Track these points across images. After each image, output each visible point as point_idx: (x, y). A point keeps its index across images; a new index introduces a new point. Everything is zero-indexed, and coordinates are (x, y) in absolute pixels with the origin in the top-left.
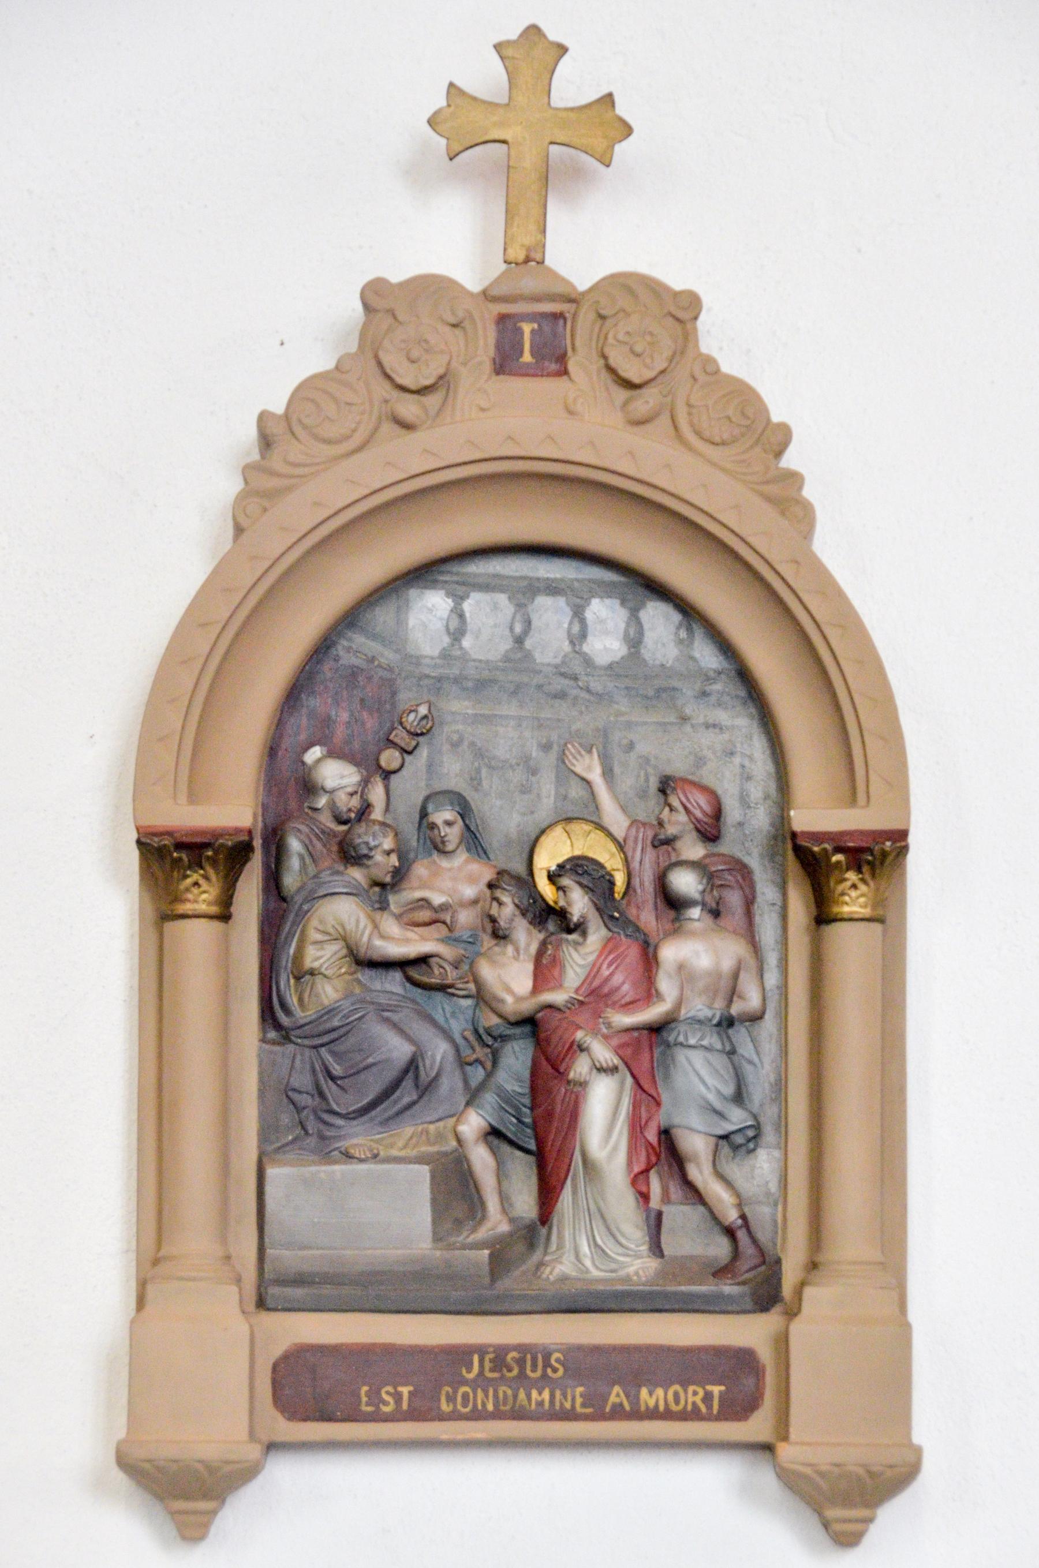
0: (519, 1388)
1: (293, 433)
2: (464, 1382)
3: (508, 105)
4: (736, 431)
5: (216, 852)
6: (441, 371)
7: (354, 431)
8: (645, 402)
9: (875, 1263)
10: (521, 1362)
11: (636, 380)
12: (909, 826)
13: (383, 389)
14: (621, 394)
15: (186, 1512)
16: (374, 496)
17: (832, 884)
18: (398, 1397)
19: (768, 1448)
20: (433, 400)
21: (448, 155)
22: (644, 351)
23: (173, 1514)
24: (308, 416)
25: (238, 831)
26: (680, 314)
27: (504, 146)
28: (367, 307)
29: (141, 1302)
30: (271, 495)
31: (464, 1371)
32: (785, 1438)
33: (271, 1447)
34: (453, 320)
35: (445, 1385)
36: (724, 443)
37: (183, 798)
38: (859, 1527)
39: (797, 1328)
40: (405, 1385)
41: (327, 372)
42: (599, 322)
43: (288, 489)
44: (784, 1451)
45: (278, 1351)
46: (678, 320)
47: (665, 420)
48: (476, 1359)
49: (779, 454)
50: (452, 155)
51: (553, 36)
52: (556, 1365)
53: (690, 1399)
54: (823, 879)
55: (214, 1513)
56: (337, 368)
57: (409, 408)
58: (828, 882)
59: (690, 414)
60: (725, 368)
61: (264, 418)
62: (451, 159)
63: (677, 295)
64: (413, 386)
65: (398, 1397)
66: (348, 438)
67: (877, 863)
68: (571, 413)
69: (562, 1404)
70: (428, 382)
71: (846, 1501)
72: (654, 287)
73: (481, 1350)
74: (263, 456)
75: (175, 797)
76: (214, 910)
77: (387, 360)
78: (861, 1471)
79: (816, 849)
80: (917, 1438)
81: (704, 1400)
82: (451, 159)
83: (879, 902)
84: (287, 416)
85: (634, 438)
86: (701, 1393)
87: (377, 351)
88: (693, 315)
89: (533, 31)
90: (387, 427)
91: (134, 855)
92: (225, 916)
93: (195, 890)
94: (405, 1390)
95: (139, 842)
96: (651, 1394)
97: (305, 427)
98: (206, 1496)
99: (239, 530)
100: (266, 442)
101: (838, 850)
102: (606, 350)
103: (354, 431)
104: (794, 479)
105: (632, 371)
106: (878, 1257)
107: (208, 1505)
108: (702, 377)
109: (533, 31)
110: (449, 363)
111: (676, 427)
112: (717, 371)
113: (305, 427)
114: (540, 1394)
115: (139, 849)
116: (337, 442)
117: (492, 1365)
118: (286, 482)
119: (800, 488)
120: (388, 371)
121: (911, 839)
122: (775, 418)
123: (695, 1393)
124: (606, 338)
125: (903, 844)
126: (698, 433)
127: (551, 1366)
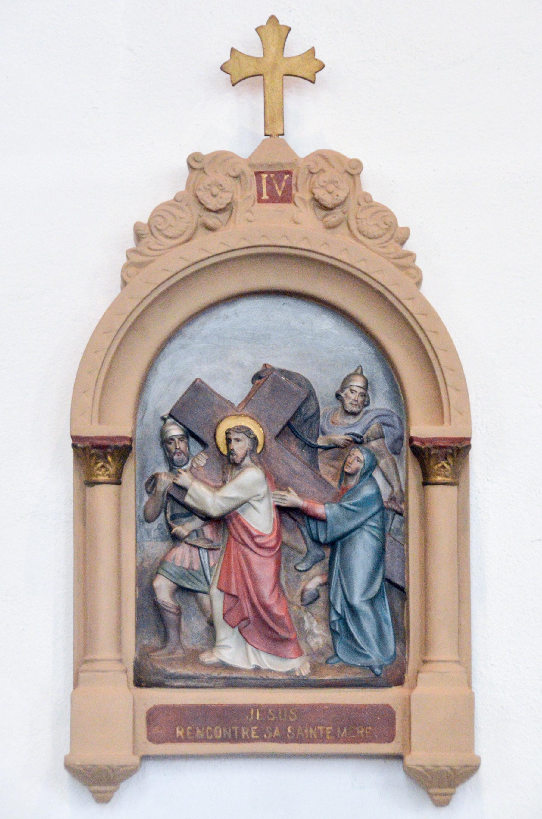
1: (152, 234)
6: (229, 201)
7: (184, 232)
8: (332, 219)
10: (277, 714)
12: (471, 434)
13: (196, 209)
15: (98, 792)
17: (432, 463)
19: (400, 757)
20: (223, 217)
22: (333, 191)
26: (353, 172)
28: (191, 168)
29: (76, 684)
30: (141, 265)
33: (145, 758)
34: (233, 174)
36: (375, 238)
37: (95, 424)
41: (345, 157)
42: (310, 175)
43: (152, 261)
47: (344, 226)
52: (292, 713)
54: (426, 461)
56: (175, 199)
57: (211, 220)
59: (357, 223)
62: (233, 85)
63: (350, 161)
64: (214, 209)
67: (455, 454)
68: (296, 223)
70: (222, 206)
71: (441, 785)
72: (339, 157)
74: (137, 246)
76: (113, 479)
77: (200, 194)
78: (447, 769)
82: (233, 85)
84: (149, 224)
90: (201, 230)
91: (70, 452)
92: (118, 482)
93: (103, 470)
95: (74, 446)
96: (314, 729)
97: (159, 230)
99: (125, 283)
100: (139, 237)
103: (184, 232)
107: (108, 788)
108: (363, 204)
110: (232, 197)
111: (349, 227)
113: (159, 230)
116: (180, 235)
119: (414, 261)
120: (202, 201)
121: (472, 442)
122: (401, 224)
124: (314, 184)
125: (467, 444)
126: (361, 232)
127: (291, 715)
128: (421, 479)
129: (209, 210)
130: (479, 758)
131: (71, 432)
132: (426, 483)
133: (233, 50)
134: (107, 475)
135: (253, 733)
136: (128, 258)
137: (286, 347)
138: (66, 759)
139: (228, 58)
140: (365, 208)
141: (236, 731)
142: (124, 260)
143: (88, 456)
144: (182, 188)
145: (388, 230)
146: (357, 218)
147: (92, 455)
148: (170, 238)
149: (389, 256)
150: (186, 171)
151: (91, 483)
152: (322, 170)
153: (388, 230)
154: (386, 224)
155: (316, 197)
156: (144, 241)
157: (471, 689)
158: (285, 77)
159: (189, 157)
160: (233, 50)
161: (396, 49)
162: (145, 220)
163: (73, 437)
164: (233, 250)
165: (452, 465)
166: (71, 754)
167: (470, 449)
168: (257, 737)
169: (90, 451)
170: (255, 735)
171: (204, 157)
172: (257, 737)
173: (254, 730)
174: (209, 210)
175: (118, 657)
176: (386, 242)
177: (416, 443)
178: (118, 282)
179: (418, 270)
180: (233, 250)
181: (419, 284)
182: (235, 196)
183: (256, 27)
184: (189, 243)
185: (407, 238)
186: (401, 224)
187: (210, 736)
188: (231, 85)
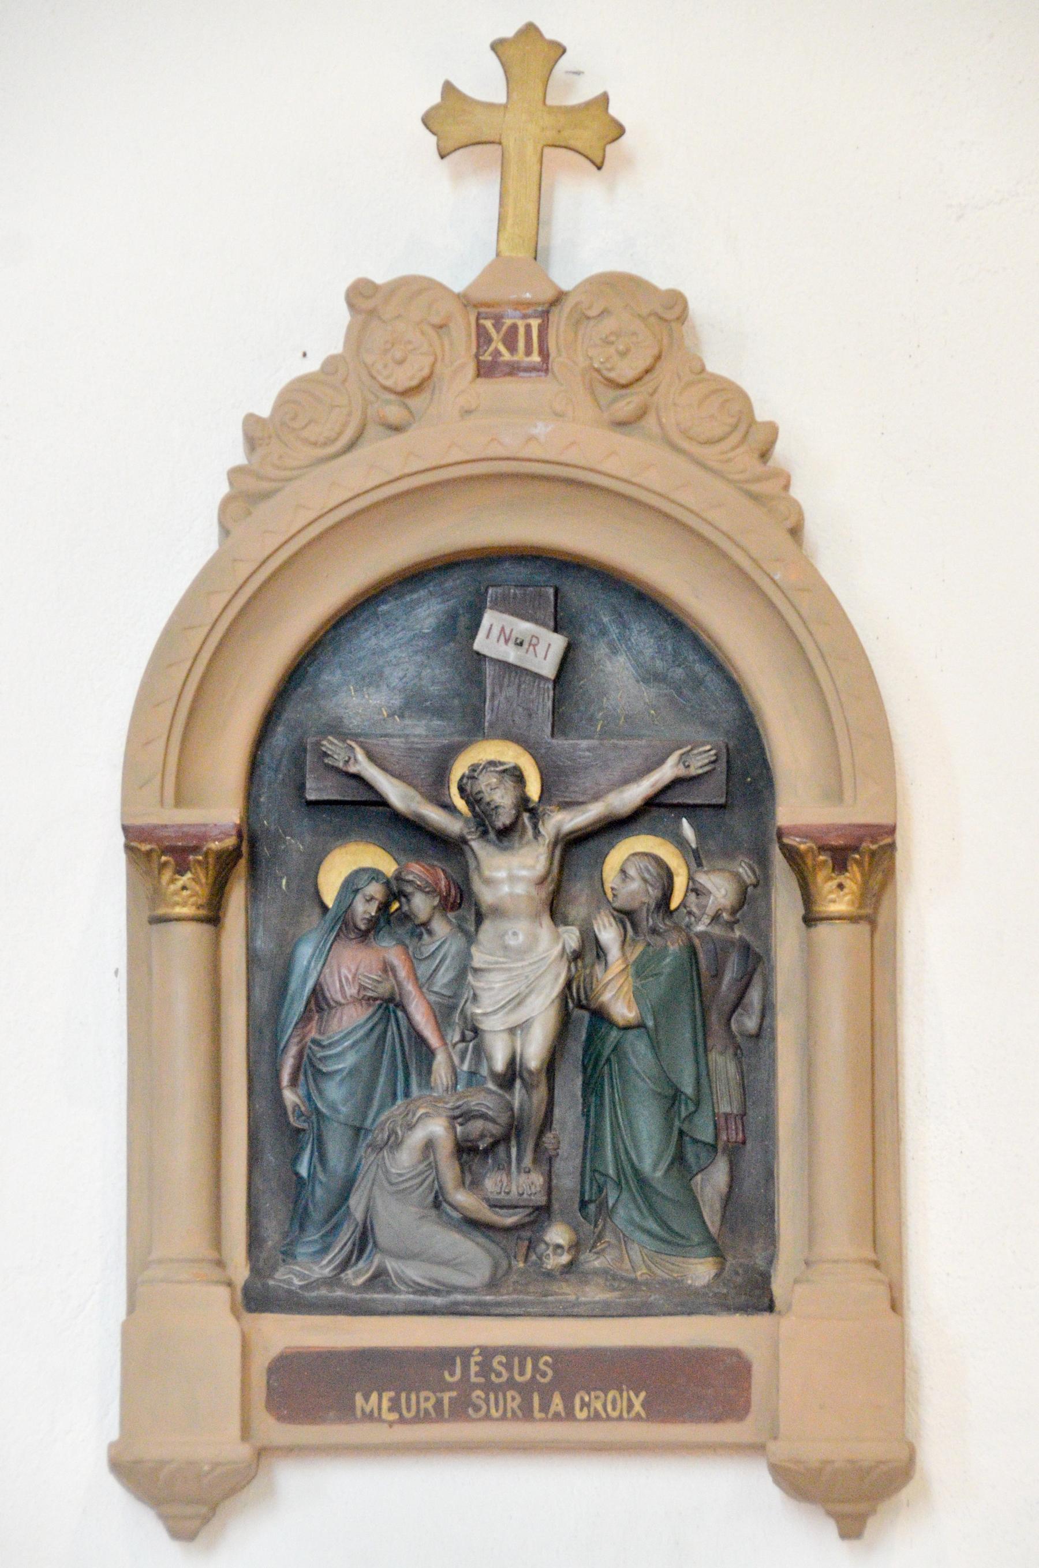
0: (371, 1392)
3: (505, 107)
4: (718, 431)
5: (206, 855)
6: (426, 372)
11: (623, 381)
16: (356, 501)
19: (756, 1449)
23: (164, 1517)
24: (294, 418)
26: (670, 315)
28: (351, 306)
33: (262, 1453)
34: (437, 320)
46: (661, 318)
48: (458, 1361)
49: (765, 455)
51: (549, 34)
53: (423, 1405)
58: (815, 878)
60: (710, 368)
61: (251, 421)
66: (340, 434)
70: (414, 383)
73: (466, 1353)
75: (162, 803)
76: (202, 912)
79: (802, 847)
81: (434, 1407)
82: (442, 157)
85: (618, 439)
86: (433, 1400)
87: (593, 366)
89: (530, 30)
91: (120, 858)
95: (129, 848)
99: (225, 531)
100: (252, 443)
101: (822, 849)
105: (626, 370)
106: (870, 1255)
109: (530, 30)
112: (703, 370)
114: (367, 1398)
115: (126, 853)
116: (325, 444)
117: (477, 1368)
118: (266, 486)
119: (786, 487)
123: (427, 1399)
127: (494, 1371)
128: (802, 911)
129: (625, 386)
132: (810, 920)
134: (193, 905)
136: (231, 483)
137: (585, 607)
138: (112, 1446)
140: (690, 384)
142: (225, 489)
143: (155, 866)
144: (337, 347)
145: (735, 427)
147: (165, 864)
148: (315, 444)
150: (342, 316)
152: (604, 313)
153: (735, 427)
154: (732, 416)
156: (260, 451)
158: (547, 150)
161: (954, 839)
162: (265, 411)
163: (125, 829)
164: (398, 479)
169: (160, 857)
170: (477, 1375)
171: (376, 288)
174: (625, 386)
176: (733, 449)
178: (215, 530)
180: (398, 479)
181: (796, 532)
182: (438, 365)
185: (772, 442)
186: (762, 414)
187: (581, 1410)
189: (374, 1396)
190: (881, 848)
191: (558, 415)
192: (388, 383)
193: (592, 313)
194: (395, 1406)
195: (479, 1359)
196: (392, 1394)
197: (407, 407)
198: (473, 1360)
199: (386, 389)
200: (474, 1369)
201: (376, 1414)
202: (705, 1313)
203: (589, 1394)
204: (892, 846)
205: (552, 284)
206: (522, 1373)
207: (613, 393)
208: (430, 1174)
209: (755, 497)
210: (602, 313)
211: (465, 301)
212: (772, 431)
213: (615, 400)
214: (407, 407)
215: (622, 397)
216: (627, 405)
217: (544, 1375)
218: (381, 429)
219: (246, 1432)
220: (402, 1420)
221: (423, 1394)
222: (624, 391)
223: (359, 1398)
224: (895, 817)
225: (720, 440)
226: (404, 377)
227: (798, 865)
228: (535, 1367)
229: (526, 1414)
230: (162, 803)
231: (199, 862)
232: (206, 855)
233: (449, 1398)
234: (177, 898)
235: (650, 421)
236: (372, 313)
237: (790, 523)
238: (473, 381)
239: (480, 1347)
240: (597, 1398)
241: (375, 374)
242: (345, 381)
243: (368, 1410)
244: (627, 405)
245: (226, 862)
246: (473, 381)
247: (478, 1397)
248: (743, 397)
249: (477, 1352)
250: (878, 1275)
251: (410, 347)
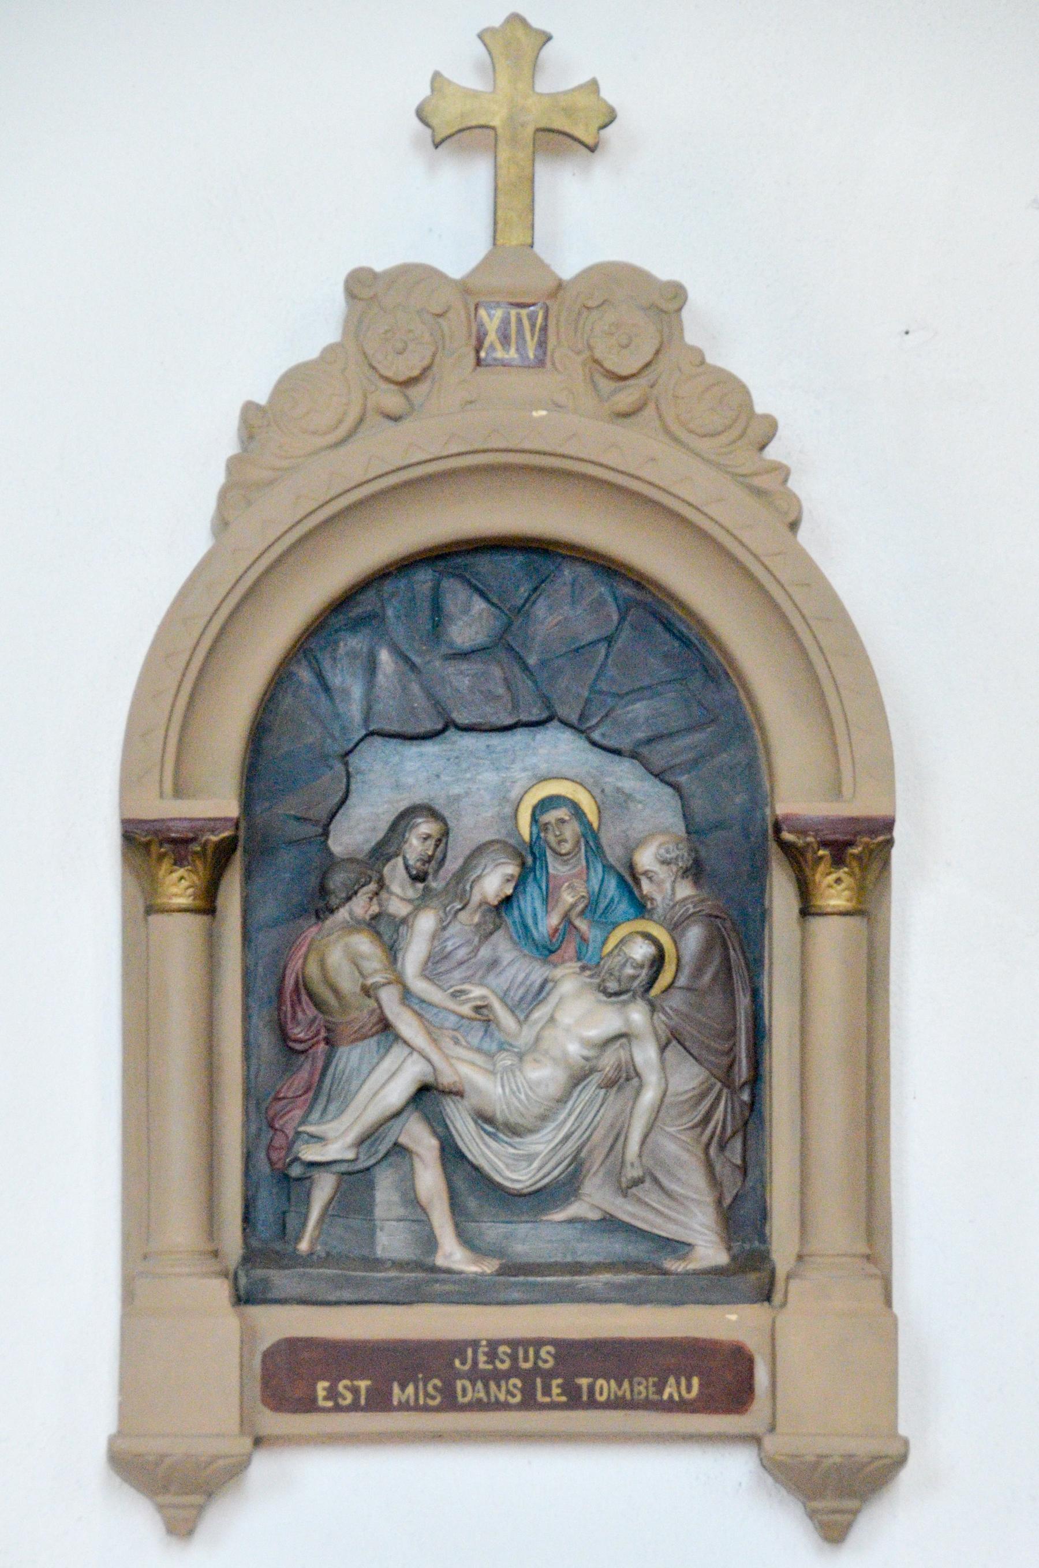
2: (460, 1375)
6: (426, 363)
9: (854, 1256)
11: (624, 372)
14: (606, 385)
18: (355, 1391)
21: (433, 141)
25: (214, 824)
26: (664, 305)
27: (492, 133)
31: (457, 1363)
32: (772, 1429)
33: (258, 1442)
35: (436, 1378)
36: (713, 435)
38: (847, 1517)
39: (784, 1320)
40: (362, 1378)
44: (770, 1443)
45: (266, 1343)
50: (438, 139)
54: (808, 872)
55: (855, 1512)
60: (709, 360)
61: (250, 410)
62: (437, 146)
65: (355, 1391)
69: (496, 1397)
70: (416, 373)
76: (199, 903)
80: (903, 1430)
82: (437, 146)
83: (861, 891)
85: (625, 434)
88: (676, 306)
89: (516, 19)
94: (363, 1384)
96: (499, 1387)
98: (852, 1494)
101: (824, 844)
102: (592, 342)
104: (782, 472)
106: (862, 1248)
107: (850, 1504)
109: (516, 19)
112: (703, 362)
114: (620, 1385)
116: (325, 433)
119: (785, 480)
121: (898, 832)
122: (759, 409)
125: (888, 837)
126: (683, 424)
127: (541, 1359)
128: (795, 906)
130: (906, 1443)
131: (121, 815)
132: (807, 911)
133: (437, 76)
135: (556, 1391)
139: (427, 92)
141: (363, 1392)
142: (219, 478)
146: (676, 397)
147: (161, 857)
149: (729, 469)
150: (337, 301)
151: (150, 910)
155: (598, 355)
157: (892, 1310)
159: (347, 282)
160: (437, 76)
165: (858, 877)
166: (121, 1433)
167: (892, 846)
168: (564, 1399)
172: (564, 1399)
173: (558, 1386)
175: (864, 1250)
177: (787, 836)
179: (794, 500)
181: (794, 526)
183: (478, 30)
184: (342, 450)
188: (431, 146)
189: (626, 1385)
190: (879, 844)
191: (558, 406)
192: (389, 374)
193: (590, 304)
194: (332, 1394)
195: (486, 1349)
196: (326, 1384)
197: (407, 397)
198: (481, 1350)
199: (387, 379)
200: (482, 1358)
201: (676, 1397)
202: (697, 1302)
203: (647, 1380)
204: (890, 843)
205: (552, 273)
206: (526, 1359)
207: (613, 385)
208: (706, 1234)
209: (759, 493)
210: (603, 304)
211: (465, 288)
212: (770, 428)
213: (614, 392)
214: (407, 397)
215: (621, 390)
216: (627, 397)
217: (546, 1361)
218: (380, 419)
219: (245, 1421)
220: (338, 1408)
221: (636, 1379)
222: (622, 384)
223: (396, 1388)
224: (895, 812)
225: (719, 433)
226: (405, 367)
227: (798, 862)
228: (537, 1356)
229: (529, 1403)
230: (162, 795)
231: (196, 853)
232: (204, 846)
233: (653, 1381)
234: (832, 891)
235: (650, 411)
236: (374, 297)
237: (791, 518)
238: (474, 370)
239: (553, 1342)
240: (639, 1384)
241: (375, 364)
242: (344, 370)
243: (404, 1398)
244: (627, 397)
245: (224, 852)
246: (474, 370)
247: (548, 1353)
248: (744, 391)
249: (484, 1343)
250: (871, 1269)
251: (411, 336)
